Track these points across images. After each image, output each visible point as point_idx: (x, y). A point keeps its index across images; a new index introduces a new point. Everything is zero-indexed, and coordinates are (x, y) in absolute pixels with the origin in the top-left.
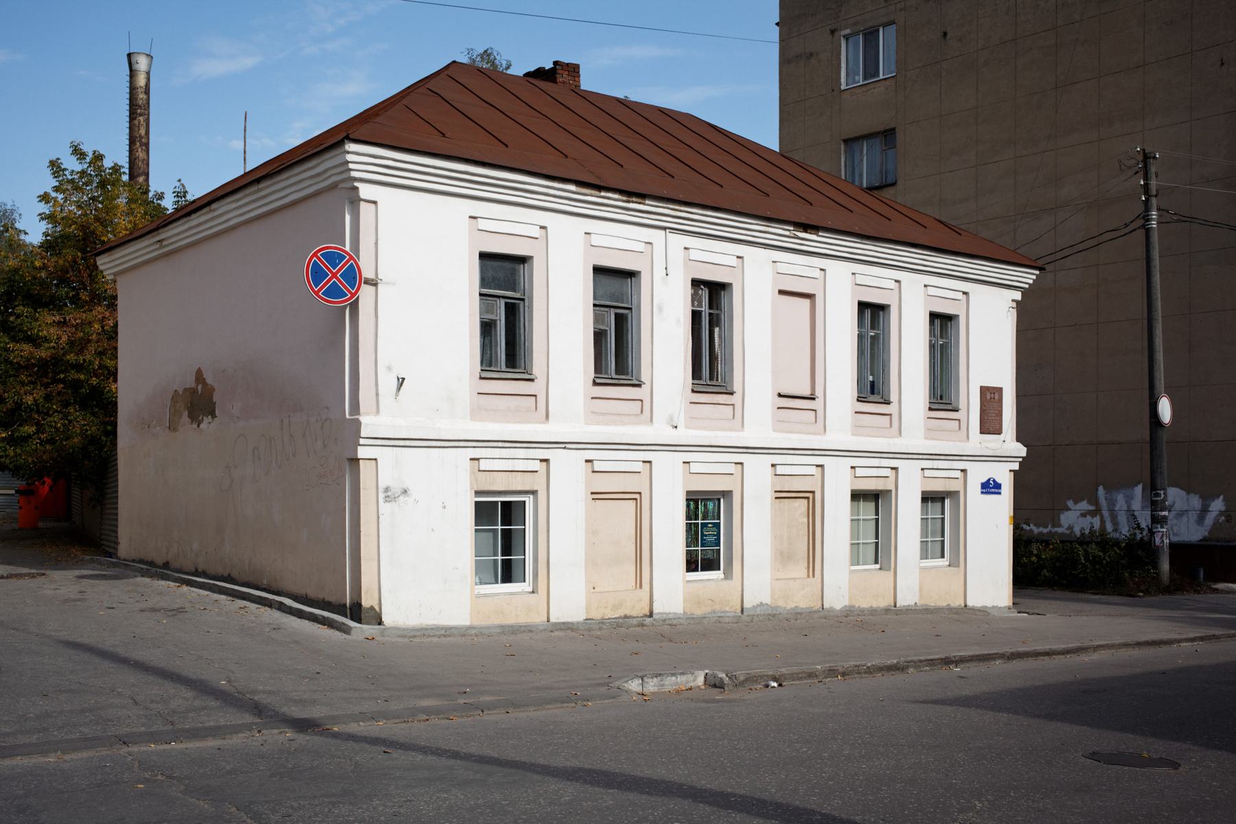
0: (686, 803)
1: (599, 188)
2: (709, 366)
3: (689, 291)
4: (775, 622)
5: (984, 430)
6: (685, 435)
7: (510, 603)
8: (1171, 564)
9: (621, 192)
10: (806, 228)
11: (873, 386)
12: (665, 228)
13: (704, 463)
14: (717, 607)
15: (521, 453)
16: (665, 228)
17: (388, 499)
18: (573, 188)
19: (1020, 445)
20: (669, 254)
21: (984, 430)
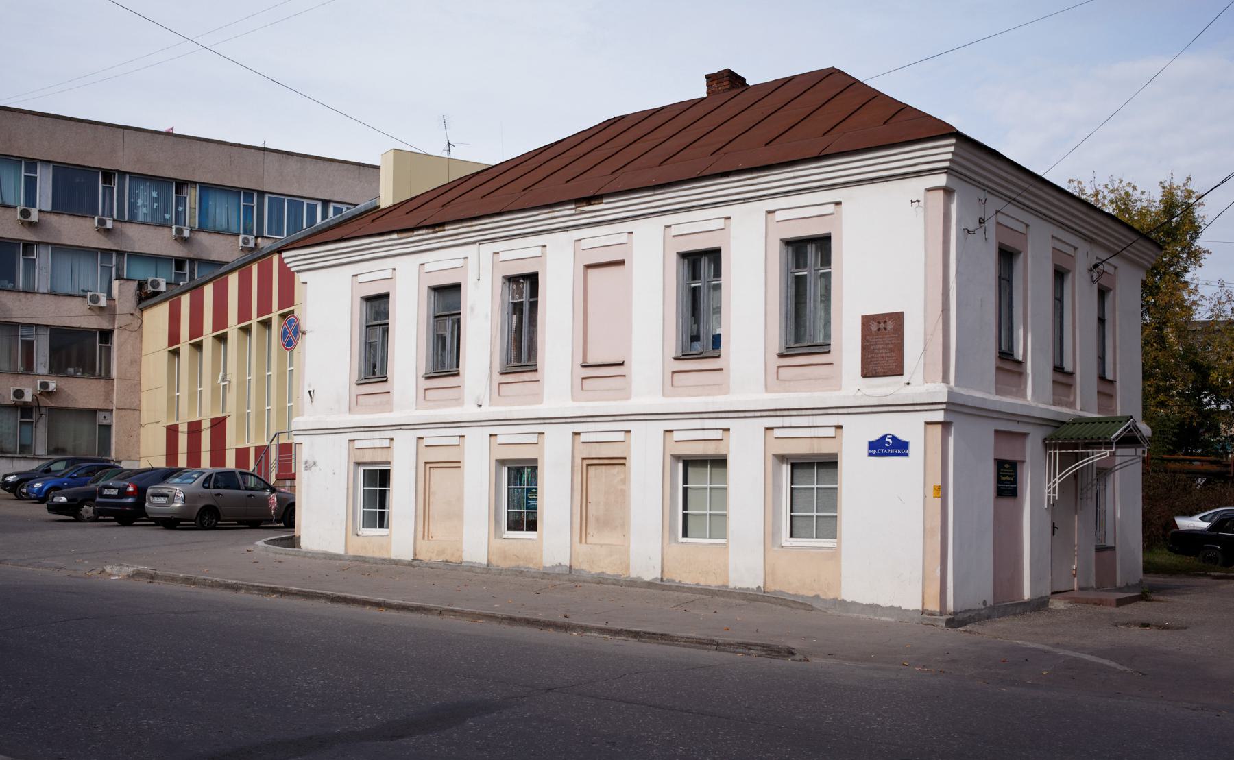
0: (389, 600)
1: (412, 230)
2: (521, 352)
3: (833, 342)
4: (568, 578)
5: (870, 370)
6: (489, 411)
7: (372, 542)
8: (1191, 514)
9: (427, 227)
10: (588, 200)
11: (699, 338)
12: (474, 243)
13: (507, 435)
14: (521, 563)
15: (377, 435)
16: (474, 243)
17: (307, 468)
18: (395, 236)
19: (130, 234)
20: (478, 264)
21: (870, 370)
